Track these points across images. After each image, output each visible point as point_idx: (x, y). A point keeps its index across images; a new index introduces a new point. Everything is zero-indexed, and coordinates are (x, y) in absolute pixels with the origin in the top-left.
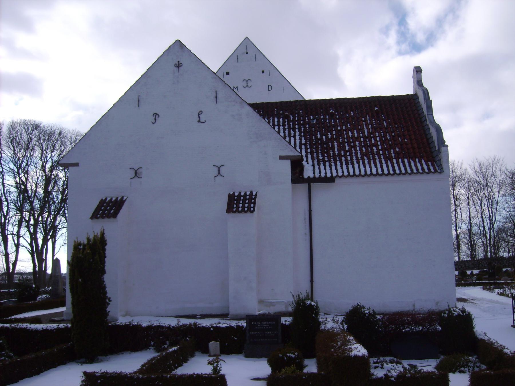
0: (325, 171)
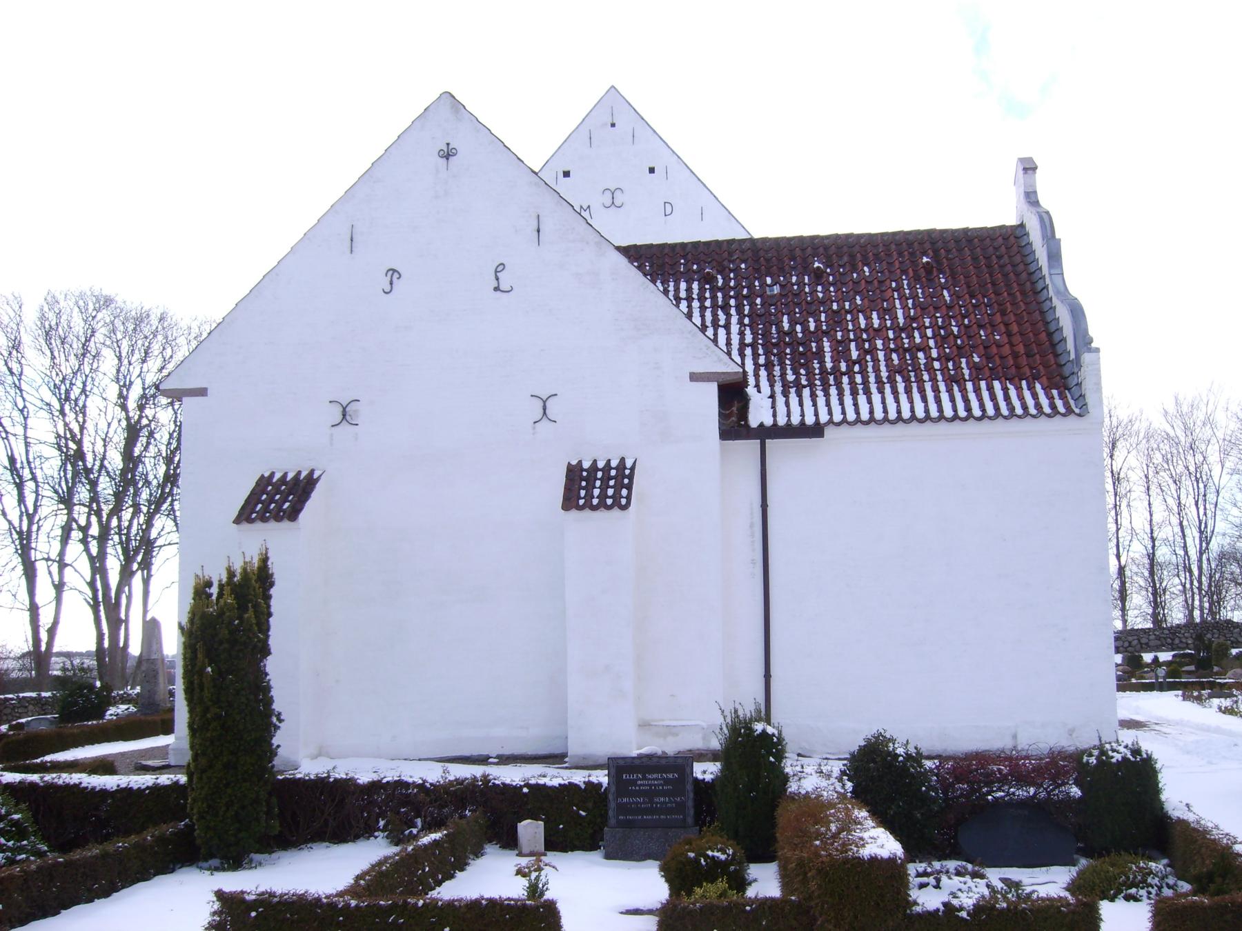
0: (801, 410)
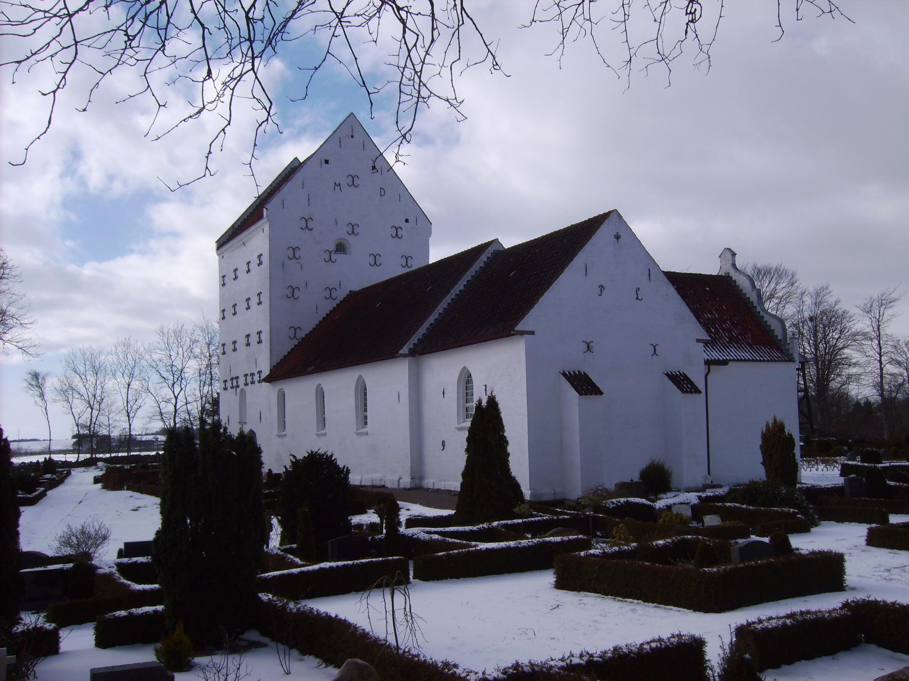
0: (715, 355)
